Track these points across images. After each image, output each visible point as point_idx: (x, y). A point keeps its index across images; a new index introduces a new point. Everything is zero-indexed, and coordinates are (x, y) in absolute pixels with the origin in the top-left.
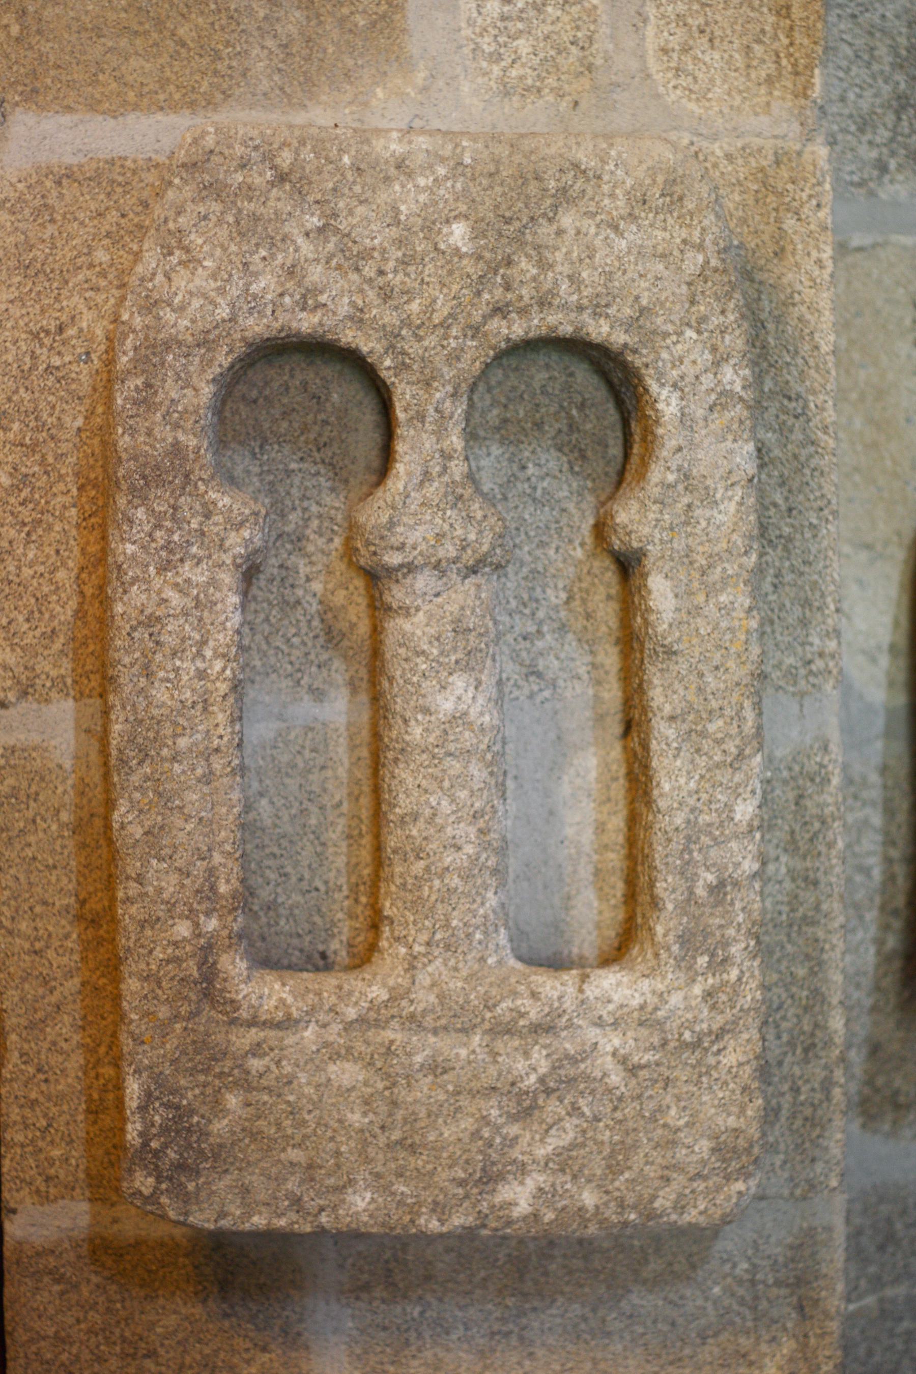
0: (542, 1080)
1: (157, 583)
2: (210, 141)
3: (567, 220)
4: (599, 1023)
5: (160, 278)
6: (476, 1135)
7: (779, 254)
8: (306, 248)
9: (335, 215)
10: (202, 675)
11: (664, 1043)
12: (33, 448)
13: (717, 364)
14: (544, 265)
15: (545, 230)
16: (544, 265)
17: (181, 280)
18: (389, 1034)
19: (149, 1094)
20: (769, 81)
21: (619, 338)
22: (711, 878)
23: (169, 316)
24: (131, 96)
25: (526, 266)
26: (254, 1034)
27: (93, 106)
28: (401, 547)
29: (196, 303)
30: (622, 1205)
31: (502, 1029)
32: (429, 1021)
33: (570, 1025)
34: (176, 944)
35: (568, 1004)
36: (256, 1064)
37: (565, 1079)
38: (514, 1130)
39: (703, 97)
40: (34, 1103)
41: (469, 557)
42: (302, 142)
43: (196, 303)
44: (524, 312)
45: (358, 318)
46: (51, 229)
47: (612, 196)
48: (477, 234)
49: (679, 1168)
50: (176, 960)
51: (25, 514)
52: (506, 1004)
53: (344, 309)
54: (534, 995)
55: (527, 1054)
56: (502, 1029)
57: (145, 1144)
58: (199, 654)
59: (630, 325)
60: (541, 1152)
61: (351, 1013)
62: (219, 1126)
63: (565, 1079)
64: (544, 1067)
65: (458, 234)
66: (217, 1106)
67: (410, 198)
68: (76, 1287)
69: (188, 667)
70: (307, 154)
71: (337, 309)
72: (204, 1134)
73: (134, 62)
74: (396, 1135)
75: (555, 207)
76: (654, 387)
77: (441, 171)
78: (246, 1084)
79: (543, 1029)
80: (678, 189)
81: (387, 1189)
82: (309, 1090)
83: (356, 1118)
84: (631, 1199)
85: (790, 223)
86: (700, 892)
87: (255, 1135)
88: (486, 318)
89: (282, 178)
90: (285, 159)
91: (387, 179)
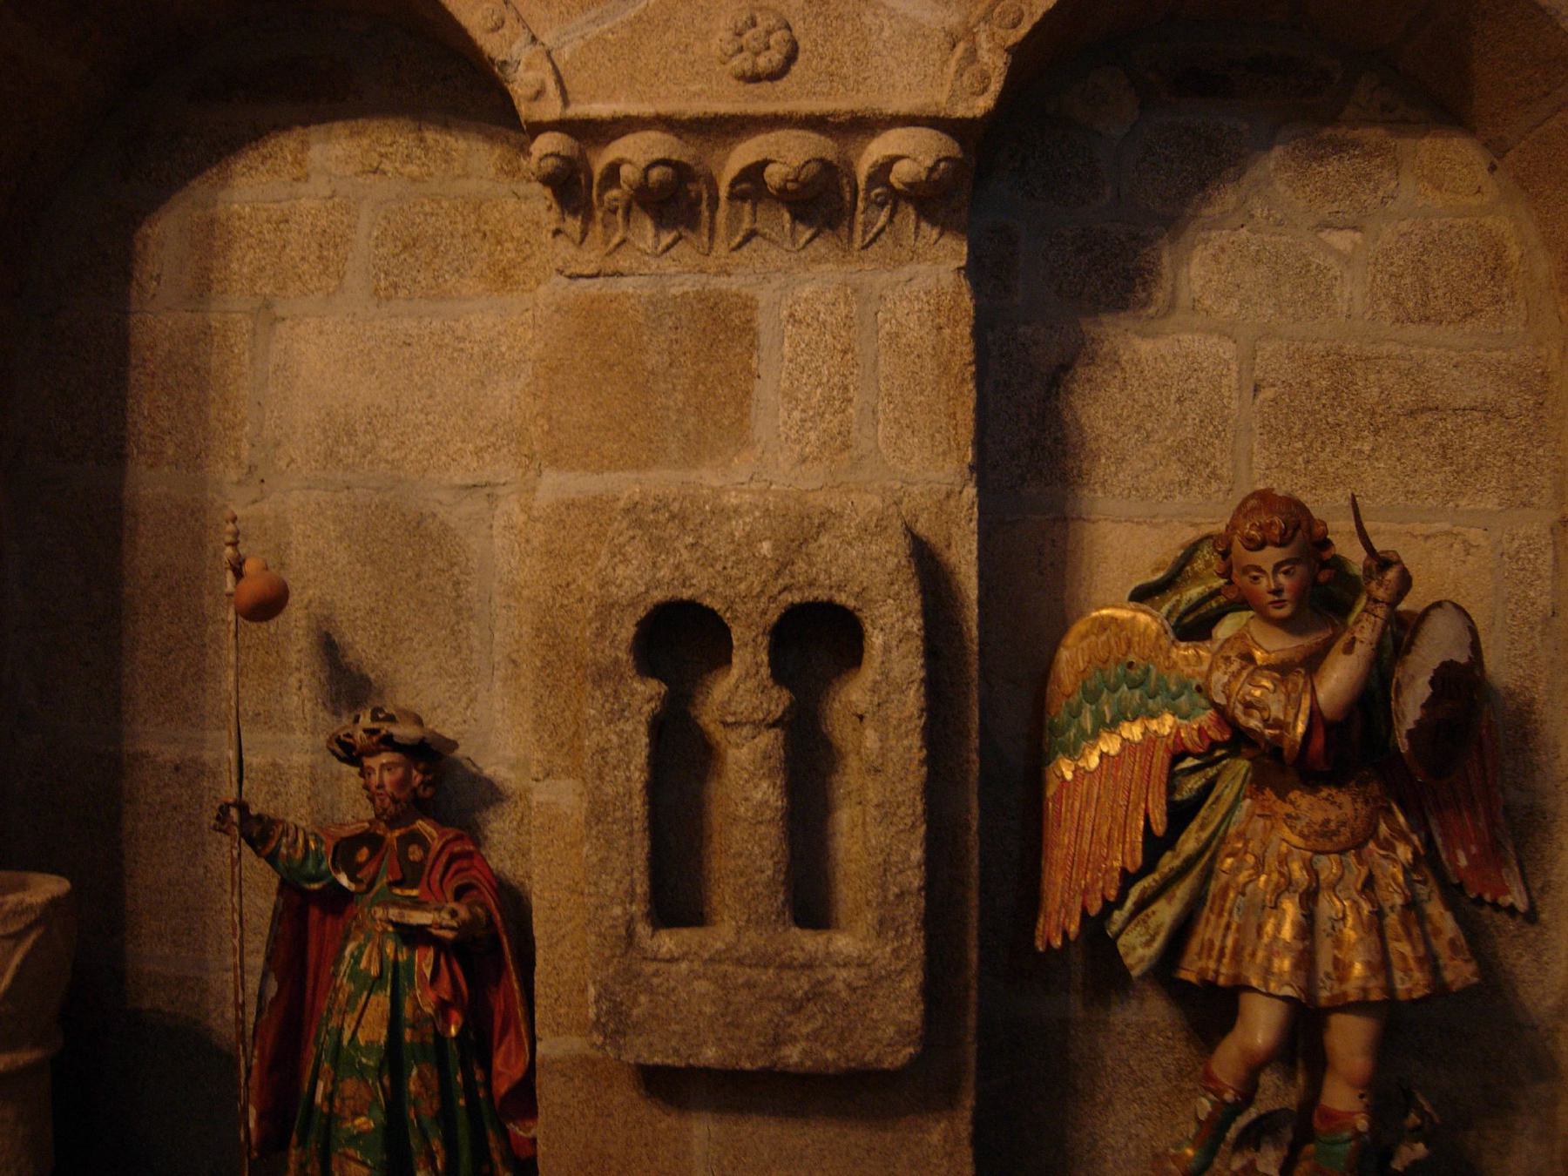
0: (806, 993)
1: (606, 730)
2: (637, 498)
3: (824, 540)
4: (837, 965)
5: (609, 569)
6: (771, 1021)
7: (948, 546)
8: (686, 555)
9: (701, 537)
10: (628, 779)
11: (870, 977)
12: (553, 647)
13: (905, 617)
14: (811, 564)
15: (813, 546)
16: (811, 564)
17: (620, 570)
18: (725, 967)
19: (600, 995)
20: (944, 453)
21: (851, 603)
22: (897, 890)
23: (614, 590)
24: (606, 462)
25: (801, 565)
26: (653, 966)
27: (586, 467)
28: (734, 714)
29: (628, 583)
30: (848, 1059)
31: (783, 966)
32: (747, 961)
33: (821, 965)
34: (614, 919)
35: (820, 955)
36: (656, 981)
37: (817, 993)
38: (788, 1019)
39: (907, 462)
40: (551, 986)
41: (770, 720)
42: (684, 498)
43: (628, 583)
44: (800, 589)
45: (711, 592)
46: (563, 533)
47: (849, 527)
48: (775, 548)
49: (878, 1041)
50: (614, 927)
51: (549, 681)
52: (788, 953)
53: (704, 588)
54: (802, 949)
55: (798, 979)
56: (783, 966)
57: (598, 1019)
58: (628, 768)
59: (857, 596)
60: (805, 1030)
61: (706, 956)
62: (635, 1012)
63: (817, 993)
64: (806, 987)
65: (766, 547)
66: (635, 1003)
67: (738, 527)
68: (572, 1079)
69: (620, 774)
70: (687, 504)
71: (701, 586)
72: (628, 1016)
73: (607, 445)
74: (729, 1019)
75: (818, 533)
76: (870, 629)
77: (757, 514)
78: (651, 990)
79: (809, 966)
80: (884, 523)
81: (725, 1047)
82: (684, 995)
83: (708, 1010)
84: (852, 1056)
85: (954, 530)
86: (891, 898)
87: (655, 1017)
88: (780, 593)
89: (673, 517)
90: (675, 507)
91: (729, 519)
